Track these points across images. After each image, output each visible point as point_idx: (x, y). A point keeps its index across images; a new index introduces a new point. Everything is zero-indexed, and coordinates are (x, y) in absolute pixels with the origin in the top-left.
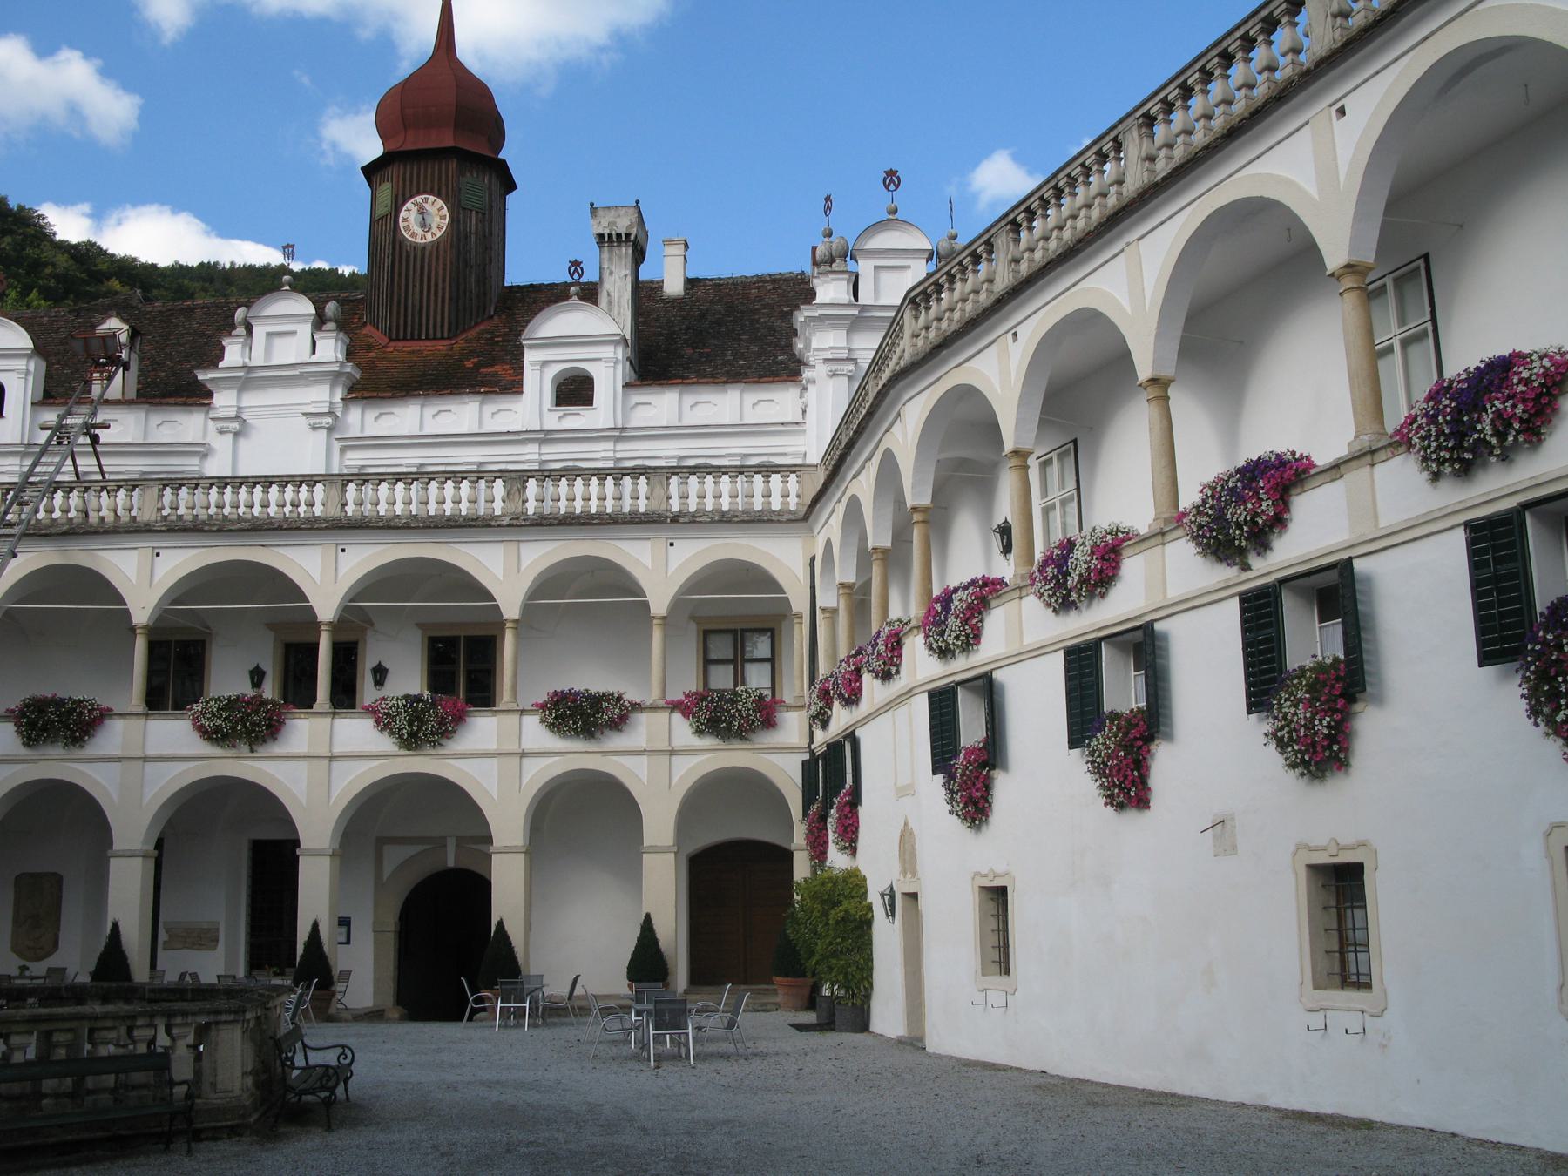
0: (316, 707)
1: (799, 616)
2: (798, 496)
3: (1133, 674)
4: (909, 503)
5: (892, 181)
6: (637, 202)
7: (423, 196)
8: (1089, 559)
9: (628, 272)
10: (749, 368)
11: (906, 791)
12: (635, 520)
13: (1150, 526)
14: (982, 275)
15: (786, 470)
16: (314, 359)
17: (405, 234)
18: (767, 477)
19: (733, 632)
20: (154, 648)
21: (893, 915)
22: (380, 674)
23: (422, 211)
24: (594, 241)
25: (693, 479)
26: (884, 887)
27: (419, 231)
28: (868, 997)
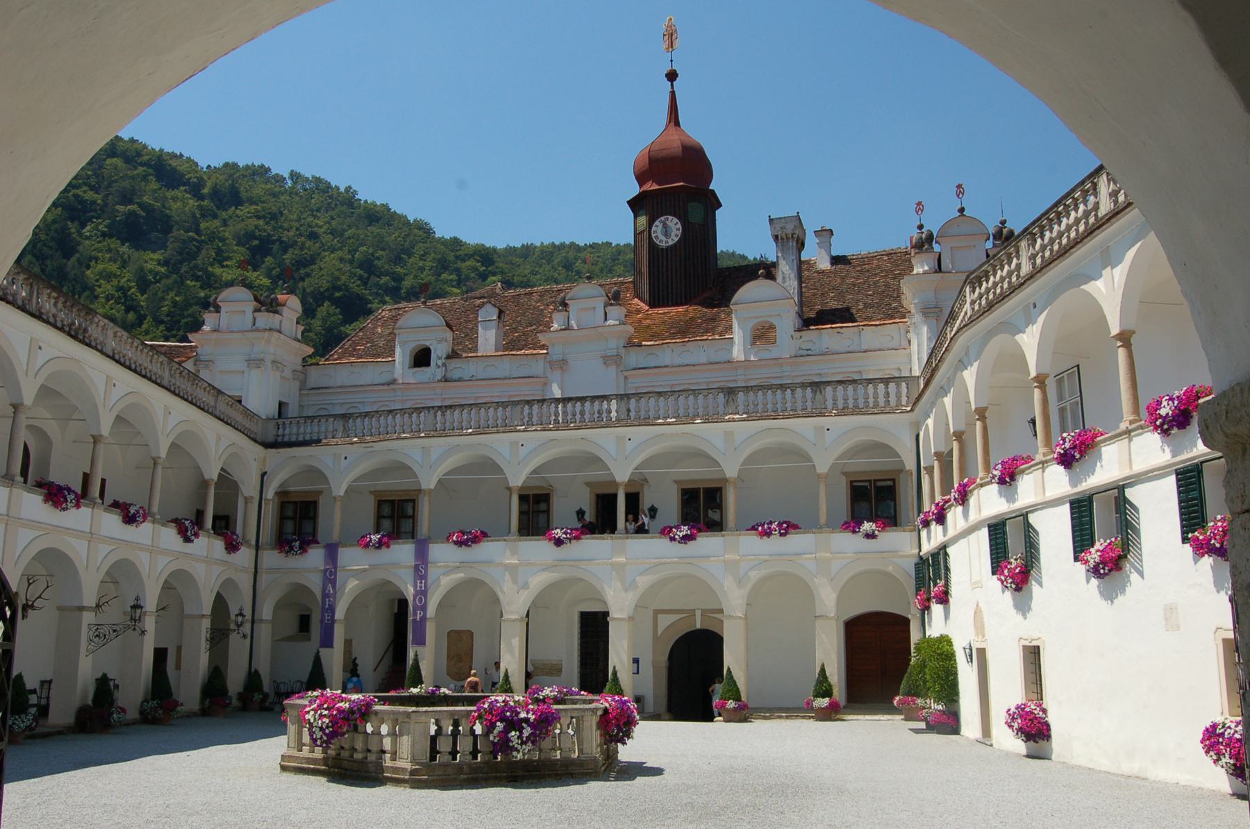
3: (1115, 515)
5: (960, 192)
6: (798, 213)
8: (991, 475)
9: (794, 257)
10: (874, 313)
11: (977, 585)
14: (1013, 265)
20: (523, 498)
21: (972, 662)
23: (665, 225)
24: (772, 239)
26: (965, 644)
27: (664, 238)
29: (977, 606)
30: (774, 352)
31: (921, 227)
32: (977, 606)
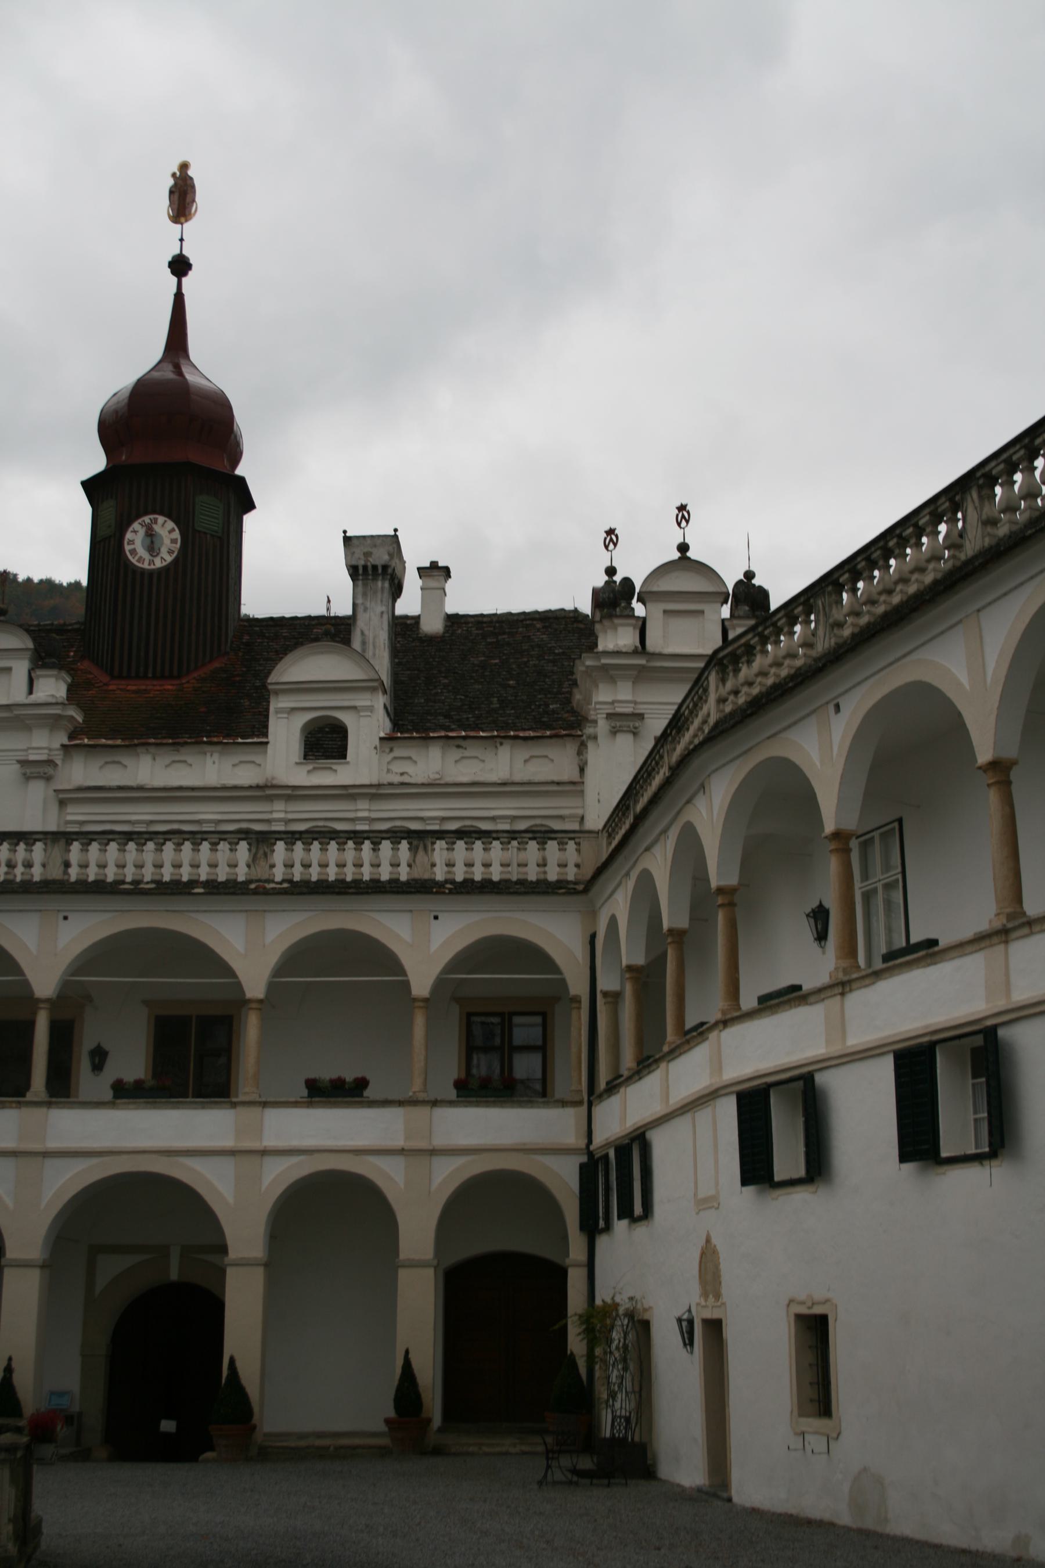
0: (29, 1096)
1: (577, 1000)
2: (577, 866)
4: (714, 883)
5: (683, 517)
6: (396, 530)
7: (152, 517)
12: (395, 888)
13: (990, 921)
15: (562, 837)
16: (33, 698)
17: (130, 558)
18: (542, 844)
19: (501, 1015)
21: (691, 1343)
22: (99, 1058)
25: (460, 845)
26: (680, 1311)
29: (708, 1241)
30: (341, 775)
31: (611, 571)
32: (708, 1241)
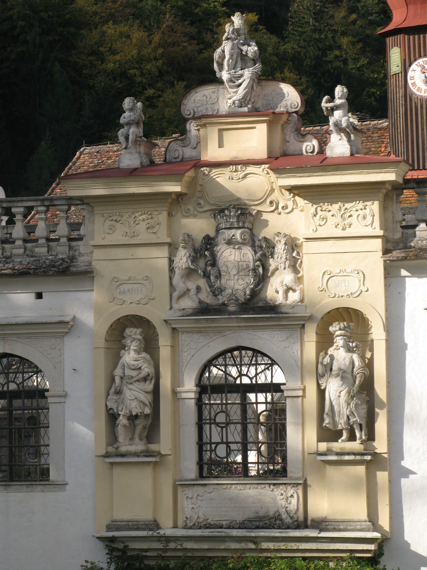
28: (287, 461)
